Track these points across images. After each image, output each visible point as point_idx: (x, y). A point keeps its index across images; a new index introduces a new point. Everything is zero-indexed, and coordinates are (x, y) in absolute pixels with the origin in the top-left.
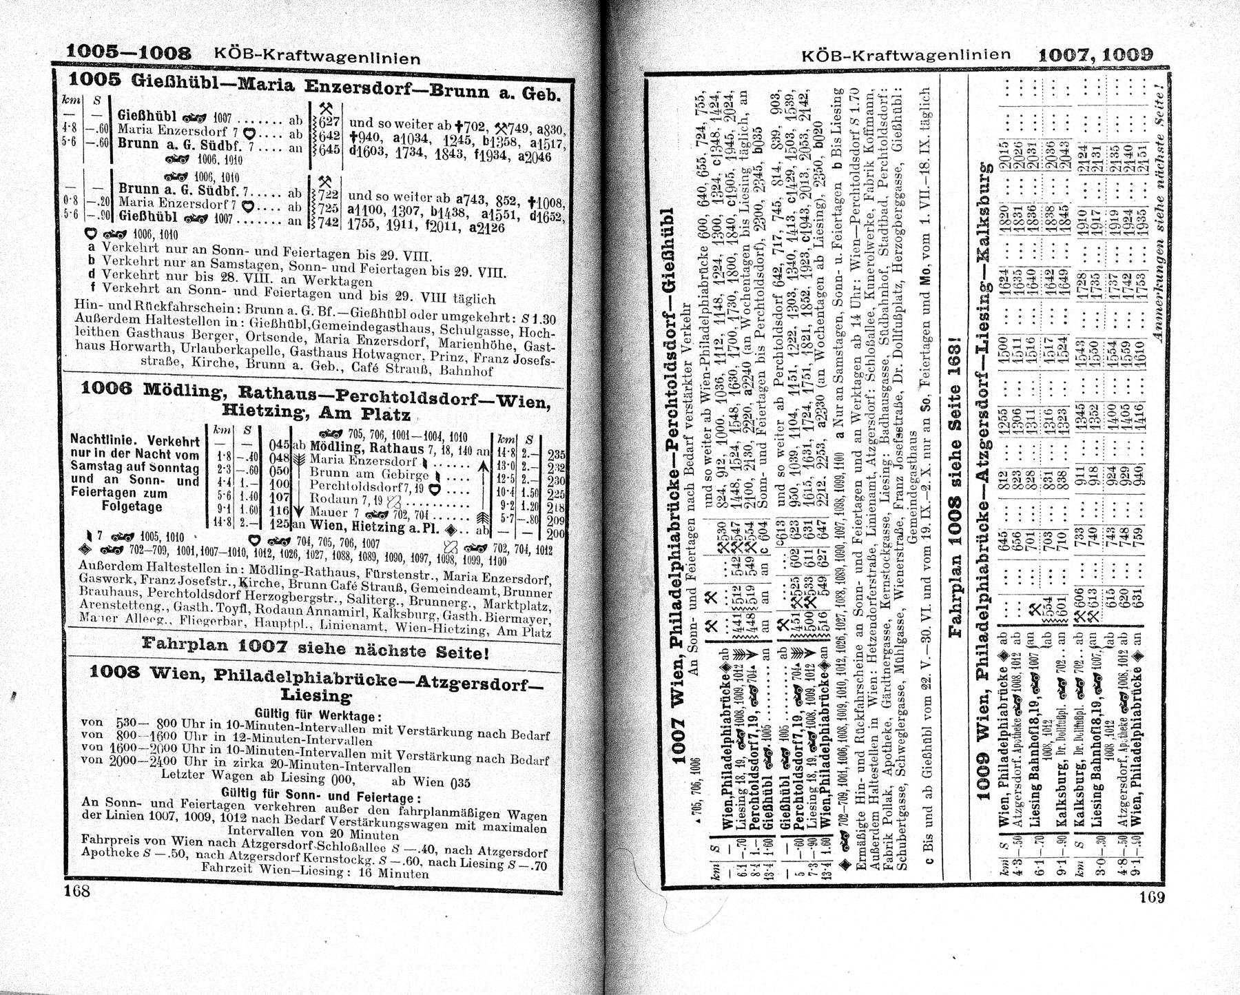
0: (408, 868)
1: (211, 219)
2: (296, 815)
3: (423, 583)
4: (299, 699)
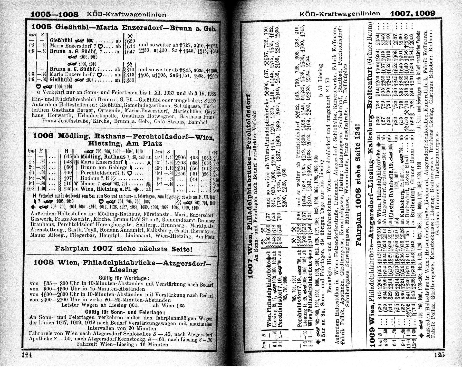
0: (160, 342)
1: (85, 80)
3: (166, 218)
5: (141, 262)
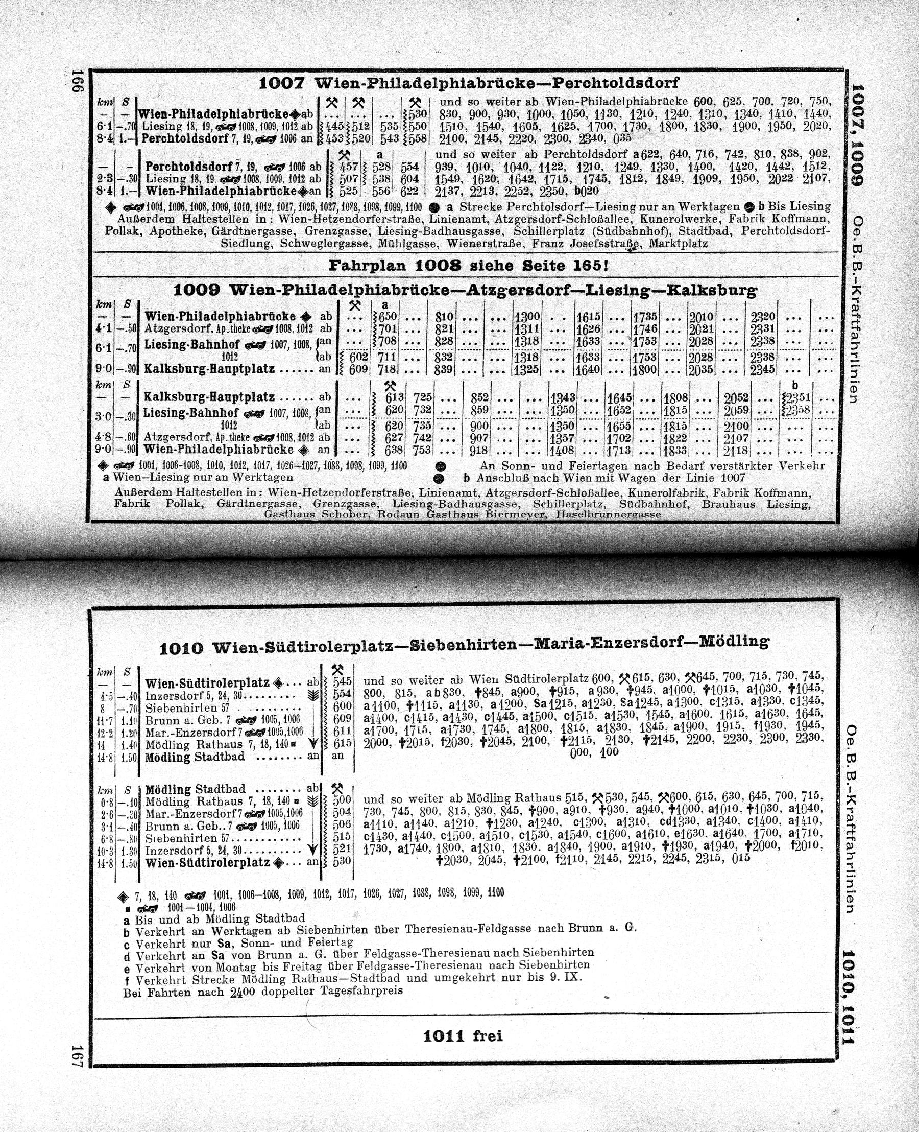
5: (283, 646)
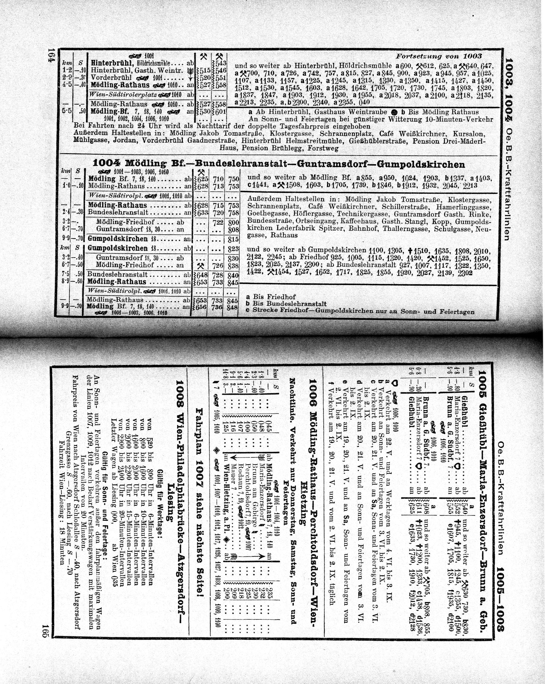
2: (94, 492)
4: (169, 493)
5: (182, 524)
